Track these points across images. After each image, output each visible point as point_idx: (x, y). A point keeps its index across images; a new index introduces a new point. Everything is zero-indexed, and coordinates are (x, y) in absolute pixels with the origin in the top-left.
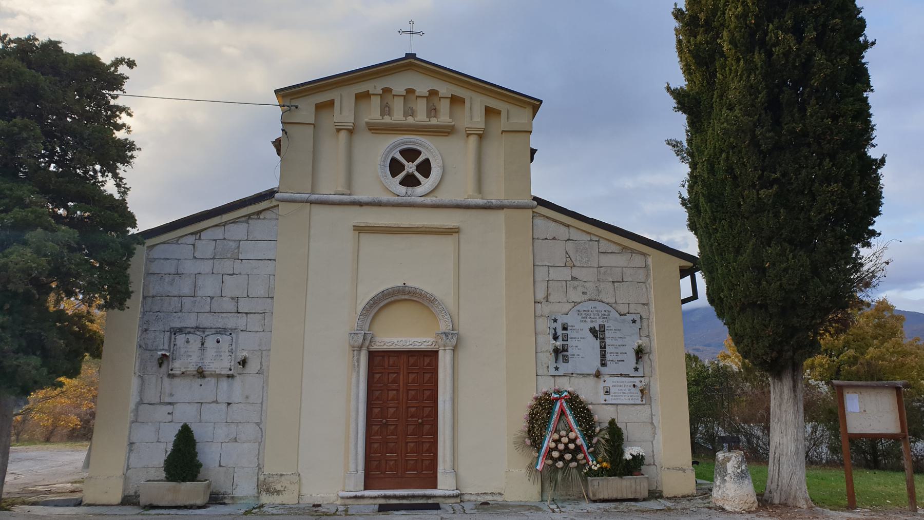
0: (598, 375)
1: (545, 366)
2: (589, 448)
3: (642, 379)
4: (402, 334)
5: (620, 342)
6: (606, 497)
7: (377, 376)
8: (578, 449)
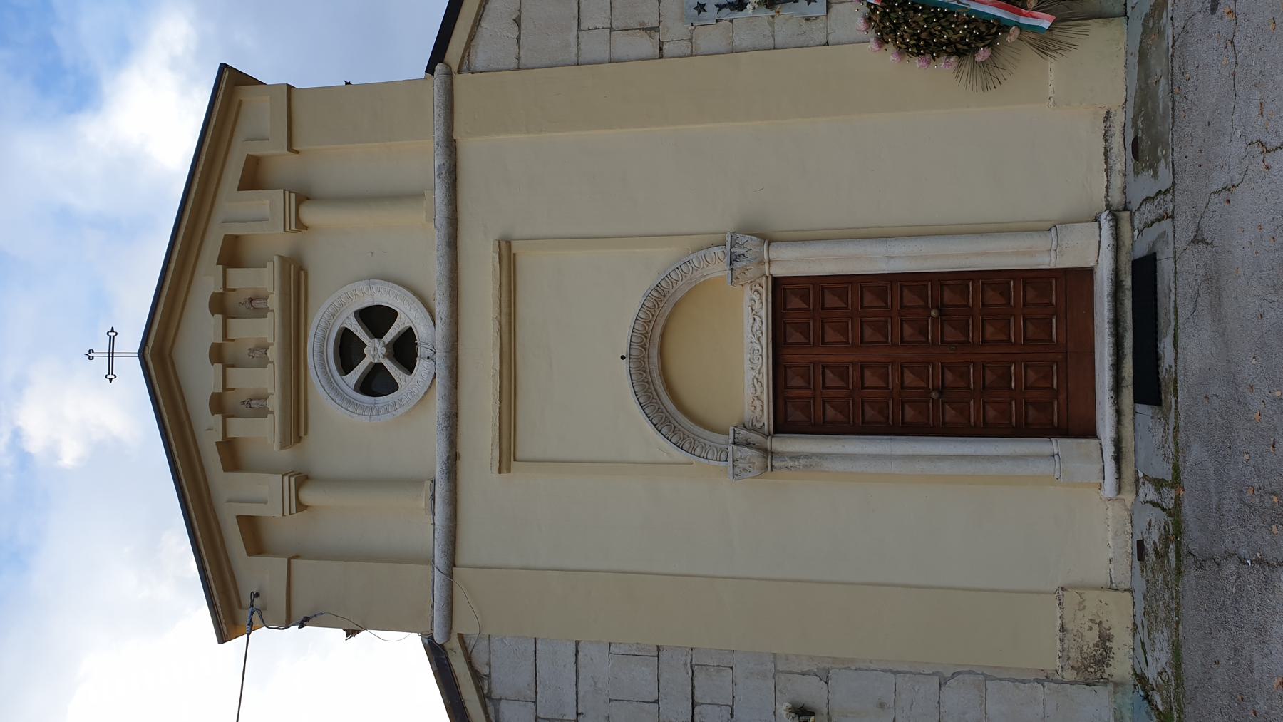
4: (735, 362)
7: (830, 412)
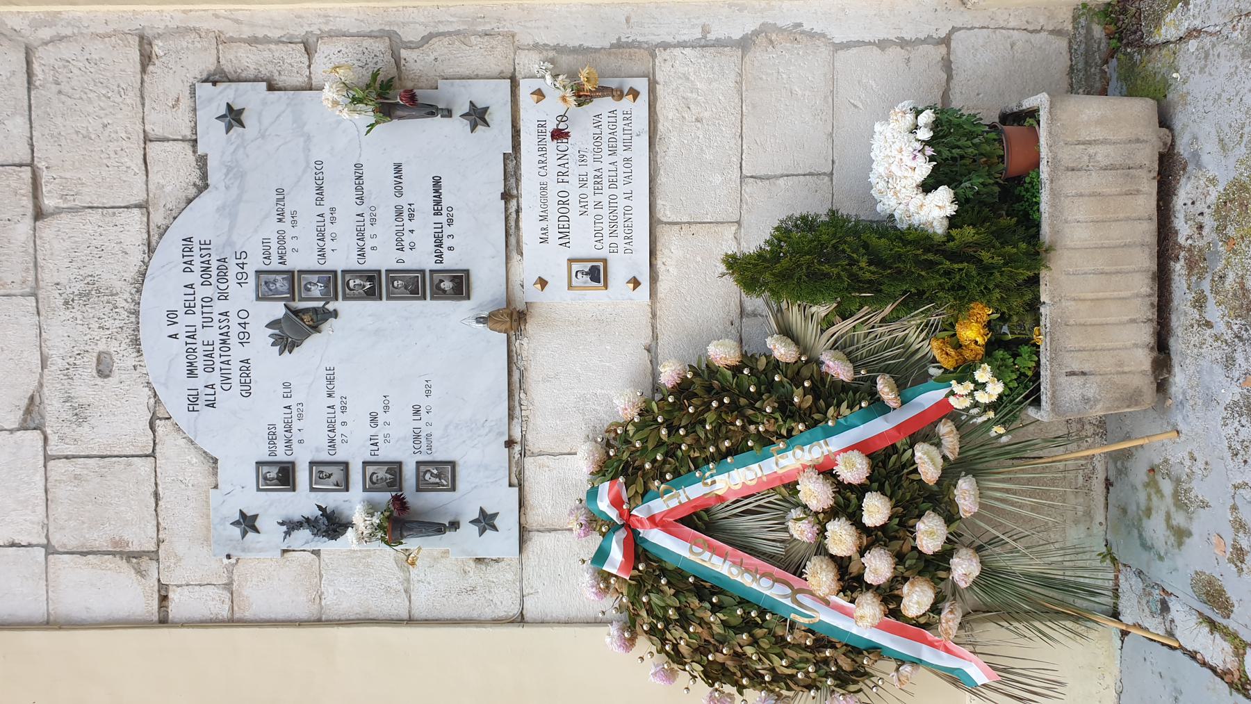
0: (512, 317)
1: (475, 576)
2: (880, 408)
3: (526, 87)
5: (341, 195)
6: (1145, 335)
8: (888, 468)
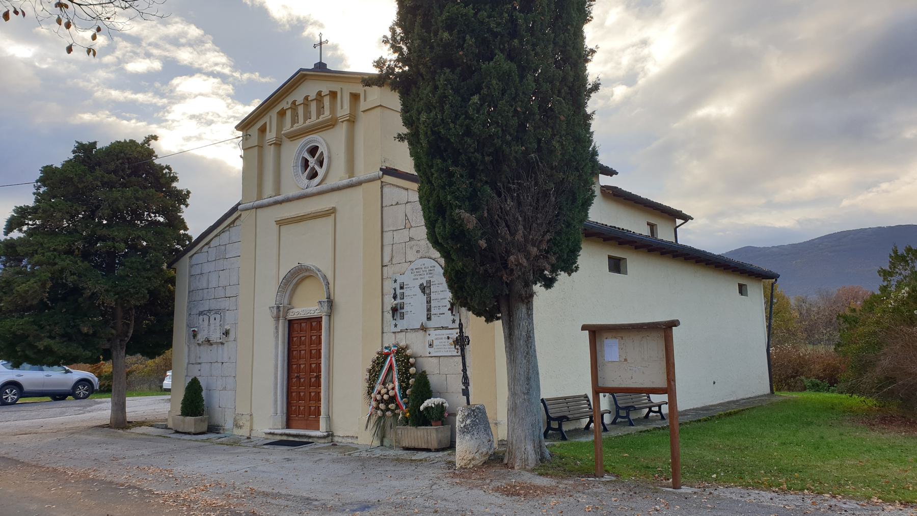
0: (424, 328)
4: (306, 306)
